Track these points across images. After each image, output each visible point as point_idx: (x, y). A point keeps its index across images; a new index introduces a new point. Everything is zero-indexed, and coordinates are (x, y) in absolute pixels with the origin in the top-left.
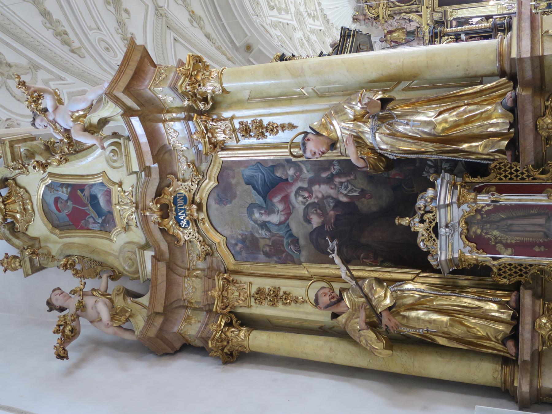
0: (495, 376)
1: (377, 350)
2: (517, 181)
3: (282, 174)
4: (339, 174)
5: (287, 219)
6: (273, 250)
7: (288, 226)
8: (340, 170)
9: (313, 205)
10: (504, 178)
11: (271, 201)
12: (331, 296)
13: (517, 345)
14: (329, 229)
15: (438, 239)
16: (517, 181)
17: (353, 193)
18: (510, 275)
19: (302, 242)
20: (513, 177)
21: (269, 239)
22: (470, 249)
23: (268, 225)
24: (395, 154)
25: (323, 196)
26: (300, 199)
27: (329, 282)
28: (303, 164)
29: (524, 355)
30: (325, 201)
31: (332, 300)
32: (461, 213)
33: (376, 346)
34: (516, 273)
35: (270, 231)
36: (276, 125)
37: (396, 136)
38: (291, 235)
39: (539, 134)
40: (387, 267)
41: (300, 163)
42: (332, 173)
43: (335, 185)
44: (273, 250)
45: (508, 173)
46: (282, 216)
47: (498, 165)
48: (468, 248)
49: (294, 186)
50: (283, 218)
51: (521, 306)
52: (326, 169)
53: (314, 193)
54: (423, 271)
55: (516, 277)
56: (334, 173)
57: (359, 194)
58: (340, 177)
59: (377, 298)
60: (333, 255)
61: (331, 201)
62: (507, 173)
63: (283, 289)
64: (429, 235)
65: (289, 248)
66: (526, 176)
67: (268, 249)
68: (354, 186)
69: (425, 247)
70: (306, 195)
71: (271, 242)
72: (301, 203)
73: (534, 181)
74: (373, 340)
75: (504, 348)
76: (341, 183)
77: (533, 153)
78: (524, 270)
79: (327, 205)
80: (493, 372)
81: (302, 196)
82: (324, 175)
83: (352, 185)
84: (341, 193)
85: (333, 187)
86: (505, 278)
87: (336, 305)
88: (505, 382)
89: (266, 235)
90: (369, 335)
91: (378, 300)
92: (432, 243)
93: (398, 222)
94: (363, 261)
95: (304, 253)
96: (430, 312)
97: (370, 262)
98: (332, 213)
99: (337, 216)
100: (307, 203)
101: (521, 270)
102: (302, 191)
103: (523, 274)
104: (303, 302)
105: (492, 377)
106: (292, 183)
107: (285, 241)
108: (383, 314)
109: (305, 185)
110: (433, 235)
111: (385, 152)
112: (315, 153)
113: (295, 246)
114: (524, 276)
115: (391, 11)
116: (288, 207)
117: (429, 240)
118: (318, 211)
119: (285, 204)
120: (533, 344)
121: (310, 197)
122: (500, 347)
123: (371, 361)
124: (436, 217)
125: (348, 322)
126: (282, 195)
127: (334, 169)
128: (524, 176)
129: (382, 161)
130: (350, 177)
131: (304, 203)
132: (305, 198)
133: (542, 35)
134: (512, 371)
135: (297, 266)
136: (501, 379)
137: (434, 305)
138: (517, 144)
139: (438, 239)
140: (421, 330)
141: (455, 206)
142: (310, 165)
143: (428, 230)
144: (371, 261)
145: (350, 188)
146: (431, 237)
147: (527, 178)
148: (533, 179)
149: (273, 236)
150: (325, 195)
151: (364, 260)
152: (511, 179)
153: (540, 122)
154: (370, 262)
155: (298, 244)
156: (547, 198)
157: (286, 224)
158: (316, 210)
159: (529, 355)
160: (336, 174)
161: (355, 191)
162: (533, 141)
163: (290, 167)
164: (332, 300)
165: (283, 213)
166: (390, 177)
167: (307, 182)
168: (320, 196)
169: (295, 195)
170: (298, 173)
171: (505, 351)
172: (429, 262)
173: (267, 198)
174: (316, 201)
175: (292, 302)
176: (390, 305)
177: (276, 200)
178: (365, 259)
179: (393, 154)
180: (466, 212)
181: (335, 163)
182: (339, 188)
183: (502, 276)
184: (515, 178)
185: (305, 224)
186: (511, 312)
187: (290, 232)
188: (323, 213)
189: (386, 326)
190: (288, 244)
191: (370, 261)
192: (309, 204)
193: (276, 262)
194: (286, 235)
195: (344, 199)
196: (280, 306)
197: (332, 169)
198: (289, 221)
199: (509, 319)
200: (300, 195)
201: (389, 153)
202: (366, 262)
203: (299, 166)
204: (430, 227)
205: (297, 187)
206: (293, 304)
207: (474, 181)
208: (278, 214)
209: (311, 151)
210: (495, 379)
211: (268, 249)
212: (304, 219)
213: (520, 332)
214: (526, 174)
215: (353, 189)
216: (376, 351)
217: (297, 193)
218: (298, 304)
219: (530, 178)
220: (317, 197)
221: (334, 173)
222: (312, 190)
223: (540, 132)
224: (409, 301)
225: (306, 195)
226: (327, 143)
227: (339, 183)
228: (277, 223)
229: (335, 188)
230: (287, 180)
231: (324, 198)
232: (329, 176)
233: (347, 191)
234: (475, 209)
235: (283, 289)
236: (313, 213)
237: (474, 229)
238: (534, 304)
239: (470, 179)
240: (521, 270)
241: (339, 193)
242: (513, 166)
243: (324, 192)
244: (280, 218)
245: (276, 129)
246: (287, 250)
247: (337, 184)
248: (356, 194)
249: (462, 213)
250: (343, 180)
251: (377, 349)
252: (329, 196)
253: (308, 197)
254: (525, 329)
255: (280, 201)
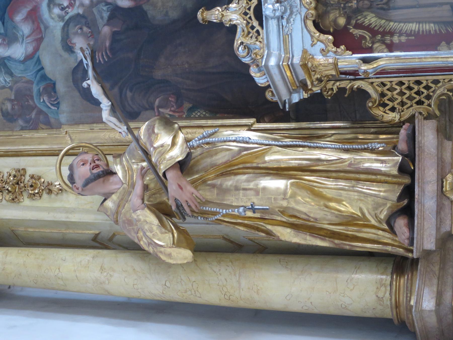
0: (381, 295)
1: (162, 249)
5: (36, 49)
6: (16, 107)
7: (39, 61)
9: (77, 18)
11: (12, 20)
12: (92, 165)
13: (411, 225)
14: (103, 58)
15: (262, 28)
18: (402, 104)
19: (61, 88)
21: (11, 88)
22: (322, 46)
23: (8, 64)
26: (56, 11)
27: (96, 146)
29: (425, 239)
30: (95, 10)
31: (95, 171)
33: (159, 240)
34: (410, 98)
35: (11, 74)
38: (44, 78)
40: (200, 118)
44: (16, 107)
46: (29, 45)
48: (320, 46)
50: (30, 49)
51: (417, 149)
54: (258, 121)
55: (411, 106)
59: (158, 147)
60: (89, 82)
61: (105, 8)
63: (30, 171)
64: (248, 23)
65: (42, 101)
67: (8, 106)
69: (245, 54)
71: (13, 92)
72: (57, 19)
74: (155, 228)
75: (393, 240)
78: (425, 91)
79: (98, 17)
80: (377, 288)
86: (393, 109)
87: (101, 180)
88: (397, 306)
89: (5, 81)
90: (148, 219)
91: (160, 152)
92: (254, 39)
93: (202, 15)
94: (159, 112)
95: (64, 106)
96: (259, 175)
97: (171, 113)
98: (106, 30)
99: (114, 34)
100: (67, 17)
101: (418, 93)
103: (423, 100)
104: (61, 190)
105: (374, 297)
107: (35, 89)
108: (168, 175)
110: (255, 23)
113: (50, 97)
114: (426, 104)
116: (39, 28)
117: (249, 33)
118: (85, 29)
119: (33, 22)
120: (440, 221)
122: (386, 237)
123: (168, 284)
125: (120, 209)
126: (29, 8)
131: (61, 18)
134: (409, 282)
135: (54, 131)
136: (391, 300)
137: (265, 162)
139: (262, 28)
140: (241, 209)
143: (246, 14)
144: (174, 111)
146: (253, 28)
149: (16, 82)
151: (161, 110)
154: (171, 113)
155: (55, 92)
157: (35, 59)
158: (81, 29)
159: (433, 240)
164: (95, 171)
165: (29, 40)
169: (49, 6)
171: (396, 244)
172: (252, 79)
173: (6, 16)
174: (81, 11)
175: (44, 192)
176: (180, 159)
177: (19, 18)
178: (162, 107)
183: (388, 108)
185: (65, 55)
186: (400, 158)
187: (42, 72)
188: (91, 32)
189: (176, 200)
190: (40, 94)
191: (171, 111)
192: (71, 19)
193: (22, 129)
194: (36, 77)
196: (26, 202)
198: (40, 53)
199: (395, 171)
202: (163, 113)
204: (249, 9)
206: (45, 195)
208: (22, 43)
210: (380, 299)
211: (8, 106)
212: (63, 47)
213: (416, 196)
216: (161, 252)
218: (53, 196)
220: (82, 5)
224: (221, 158)
228: (22, 59)
235: (30, 171)
236: (76, 33)
237: (332, 16)
238: (440, 147)
240: (418, 93)
244: (26, 49)
246: (38, 105)
251: (161, 246)
253: (68, 7)
254: (426, 193)
255: (26, 19)
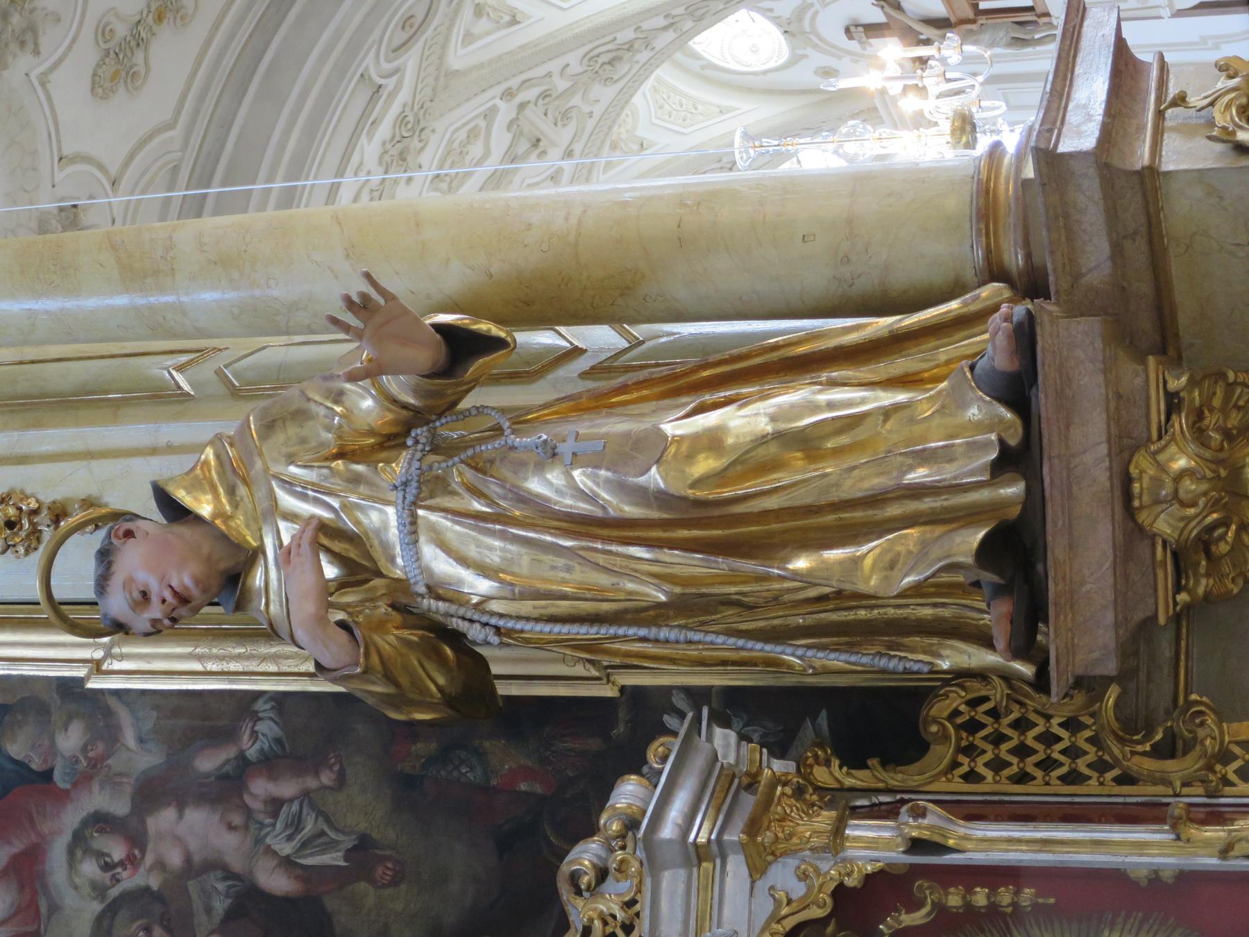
2: (1047, 789)
3: (33, 747)
4: (270, 763)
8: (278, 741)
10: (989, 774)
16: (1047, 789)
17: (322, 852)
20: (1031, 769)
24: (493, 621)
25: (188, 860)
26: (90, 868)
28: (127, 704)
30: (192, 885)
32: (765, 907)
36: (34, 505)
37: (466, 448)
39: (1140, 529)
41: (113, 702)
42: (242, 757)
43: (248, 812)
45: (1010, 752)
47: (963, 708)
49: (70, 807)
52: (221, 735)
53: (151, 846)
56: (252, 753)
57: (346, 858)
58: (273, 776)
61: (221, 886)
62: (1005, 747)
66: (1089, 766)
68: (328, 821)
70: (117, 852)
72: (87, 890)
73: (1126, 789)
76: (275, 805)
77: (1109, 617)
79: (198, 905)
81: (100, 855)
82: (208, 762)
83: (320, 813)
84: (270, 851)
85: (237, 819)
100: (114, 892)
102: (101, 831)
106: (67, 792)
109: (120, 807)
111: (453, 609)
112: (145, 595)
115: (1065, 561)
116: (33, 905)
119: (22, 887)
121: (131, 861)
124: (638, 915)
127: (254, 735)
128: (1082, 765)
129: (441, 660)
130: (317, 774)
131: (99, 890)
132: (107, 867)
133: (1160, 114)
138: (1040, 567)
141: (736, 866)
142: (155, 714)
145: (309, 827)
147: (1095, 775)
148: (1119, 781)
150: (197, 859)
152: (1022, 778)
153: (1142, 465)
156: (1172, 836)
160: (260, 761)
161: (331, 845)
162: (1110, 552)
163: (70, 718)
166: (494, 782)
167: (128, 789)
168: (175, 859)
169: (71, 851)
170: (100, 747)
174: (154, 882)
179: (484, 619)
180: (789, 902)
181: (260, 706)
182: (262, 825)
184: (1039, 774)
192: (128, 898)
195: (277, 882)
197: (246, 737)
200: (88, 851)
201: (469, 615)
203: (108, 713)
205: (83, 814)
207: (849, 782)
209: (128, 583)
214: (1091, 758)
215: (322, 834)
217: (79, 840)
219: (1110, 775)
220: (160, 865)
221: (252, 753)
222: (145, 832)
223: (1143, 517)
225: (117, 852)
226: (209, 559)
227: (265, 802)
229: (246, 827)
230: (47, 775)
231: (193, 869)
232: (228, 768)
233: (296, 843)
234: (833, 885)
239: (837, 773)
241: (262, 849)
242: (1033, 717)
243: (193, 844)
245: (31, 523)
247: (256, 805)
248: (334, 858)
249: (769, 906)
250: (287, 788)
252: (214, 865)
253: (121, 863)
